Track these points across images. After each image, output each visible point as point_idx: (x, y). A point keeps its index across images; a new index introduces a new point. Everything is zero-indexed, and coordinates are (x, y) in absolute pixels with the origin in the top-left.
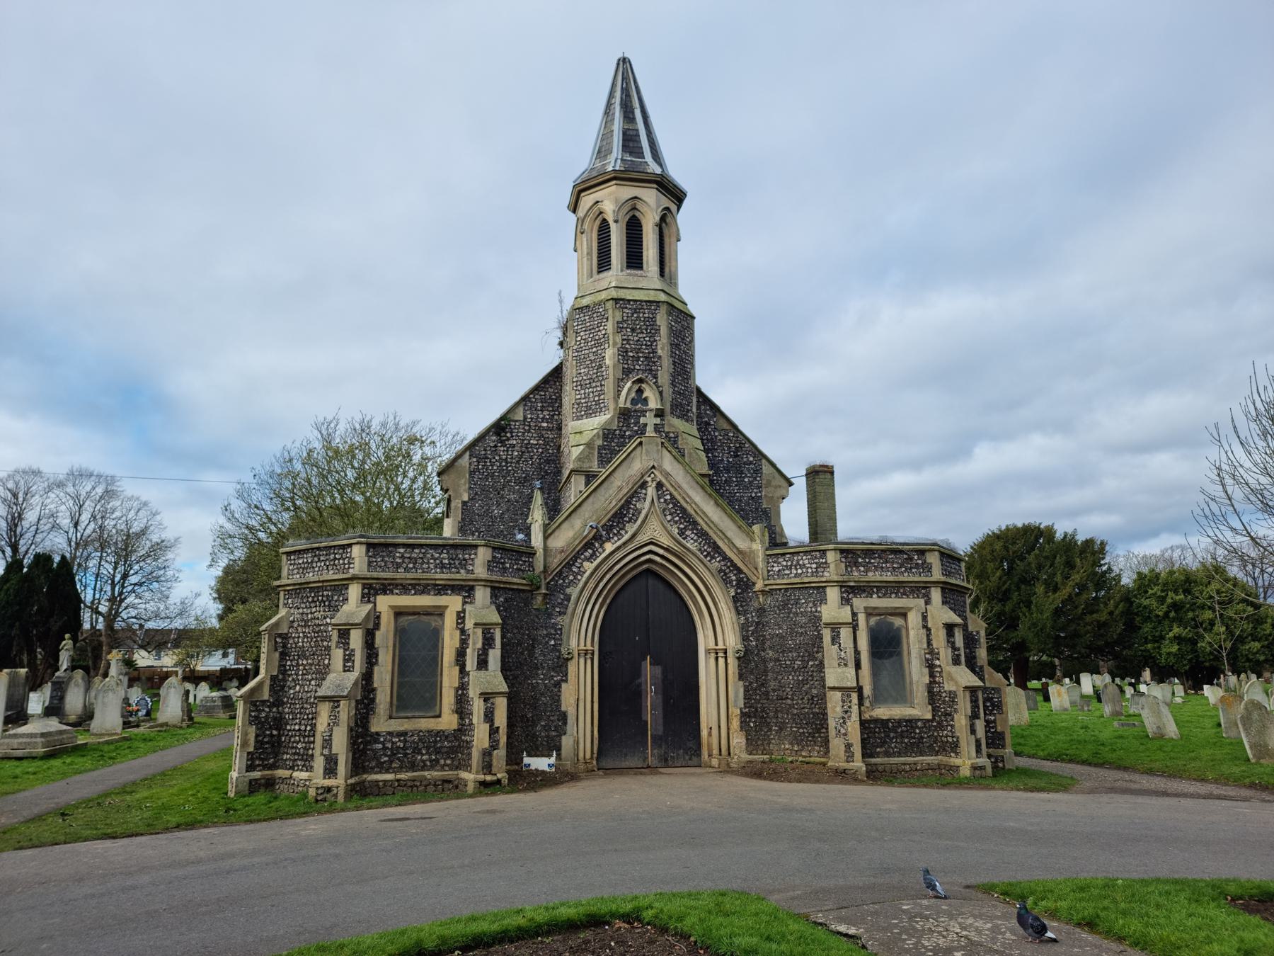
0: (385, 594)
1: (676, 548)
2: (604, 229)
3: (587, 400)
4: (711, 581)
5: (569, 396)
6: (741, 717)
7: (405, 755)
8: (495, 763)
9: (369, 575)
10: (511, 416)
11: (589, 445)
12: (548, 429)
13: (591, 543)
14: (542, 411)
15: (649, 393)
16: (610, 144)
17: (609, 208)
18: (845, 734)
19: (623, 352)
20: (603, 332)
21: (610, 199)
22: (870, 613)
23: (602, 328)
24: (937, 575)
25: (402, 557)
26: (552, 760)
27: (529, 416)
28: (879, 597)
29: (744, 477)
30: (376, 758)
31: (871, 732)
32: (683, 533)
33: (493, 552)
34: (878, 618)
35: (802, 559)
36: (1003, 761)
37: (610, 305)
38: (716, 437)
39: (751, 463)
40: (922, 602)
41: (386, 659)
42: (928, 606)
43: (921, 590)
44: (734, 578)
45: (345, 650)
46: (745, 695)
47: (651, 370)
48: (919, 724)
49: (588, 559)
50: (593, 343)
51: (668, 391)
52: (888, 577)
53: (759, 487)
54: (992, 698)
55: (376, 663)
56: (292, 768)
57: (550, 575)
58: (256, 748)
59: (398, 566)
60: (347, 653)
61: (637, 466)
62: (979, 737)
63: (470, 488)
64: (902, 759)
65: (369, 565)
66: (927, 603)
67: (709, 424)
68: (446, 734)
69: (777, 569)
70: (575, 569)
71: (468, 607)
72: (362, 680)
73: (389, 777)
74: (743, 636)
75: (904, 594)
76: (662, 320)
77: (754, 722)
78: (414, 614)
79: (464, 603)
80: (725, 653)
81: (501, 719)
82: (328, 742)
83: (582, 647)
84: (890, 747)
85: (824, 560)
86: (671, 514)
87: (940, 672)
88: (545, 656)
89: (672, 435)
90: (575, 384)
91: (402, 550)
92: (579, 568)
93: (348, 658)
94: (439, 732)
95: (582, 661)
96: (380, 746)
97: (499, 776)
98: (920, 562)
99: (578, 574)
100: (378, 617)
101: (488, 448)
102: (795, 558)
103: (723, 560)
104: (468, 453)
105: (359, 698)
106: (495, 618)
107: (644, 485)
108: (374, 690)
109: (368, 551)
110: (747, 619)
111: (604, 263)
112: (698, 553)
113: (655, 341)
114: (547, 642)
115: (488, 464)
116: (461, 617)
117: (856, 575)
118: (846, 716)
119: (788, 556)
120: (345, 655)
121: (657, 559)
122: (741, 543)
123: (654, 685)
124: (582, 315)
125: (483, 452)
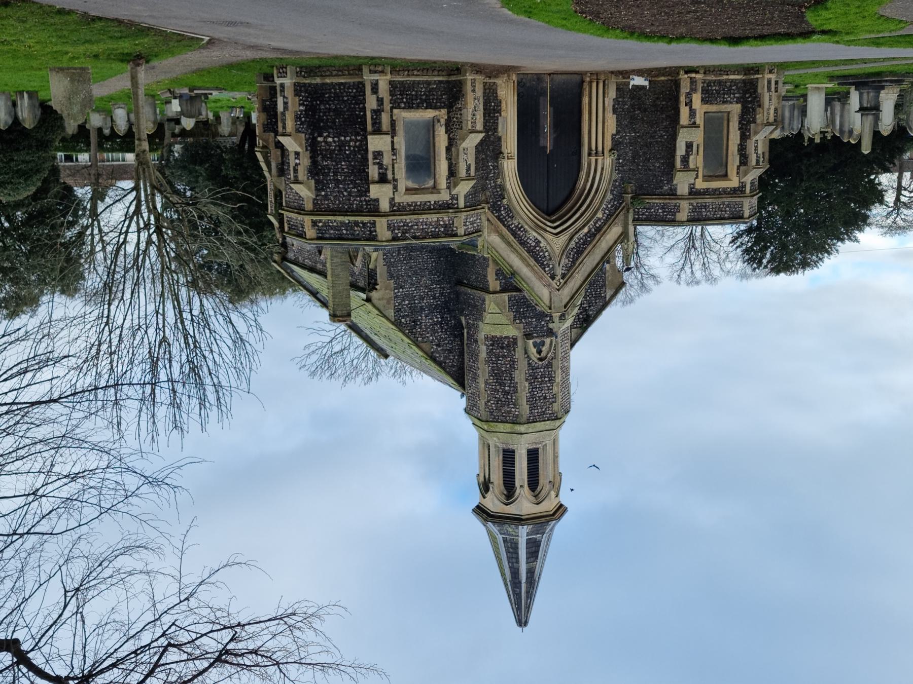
0: (734, 188)
1: (542, 232)
2: (533, 482)
6: (500, 110)
7: (723, 90)
8: (688, 84)
9: (742, 199)
10: (580, 331)
13: (598, 232)
18: (475, 99)
22: (435, 189)
24: (381, 224)
25: (726, 211)
26: (632, 83)
28: (430, 202)
29: (409, 304)
30: (738, 88)
31: (440, 99)
32: (537, 243)
33: (675, 218)
34: (426, 186)
36: (297, 73)
38: (431, 335)
39: (403, 317)
40: (397, 200)
42: (392, 196)
43: (397, 209)
44: (503, 212)
46: (497, 126)
47: (533, 369)
48: (403, 105)
49: (599, 219)
53: (396, 297)
54: (300, 124)
55: (738, 145)
57: (624, 207)
59: (728, 206)
62: (381, 96)
63: (605, 274)
64: (417, 79)
65: (742, 205)
66: (393, 199)
67: (437, 345)
70: (607, 212)
71: (693, 181)
72: (750, 135)
73: (732, 77)
74: (498, 169)
75: (410, 206)
76: (524, 409)
77: (491, 106)
79: (694, 184)
81: (684, 112)
83: (593, 159)
84: (425, 88)
86: (545, 257)
88: (625, 152)
89: (518, 321)
91: (726, 216)
95: (600, 149)
96: (736, 95)
97: (686, 76)
98: (396, 231)
99: (605, 209)
100: (738, 173)
103: (510, 225)
104: (607, 299)
105: (752, 125)
108: (739, 129)
109: (743, 214)
110: (495, 182)
111: (533, 456)
112: (529, 229)
113: (530, 393)
114: (624, 160)
117: (445, 218)
121: (549, 224)
123: (544, 133)
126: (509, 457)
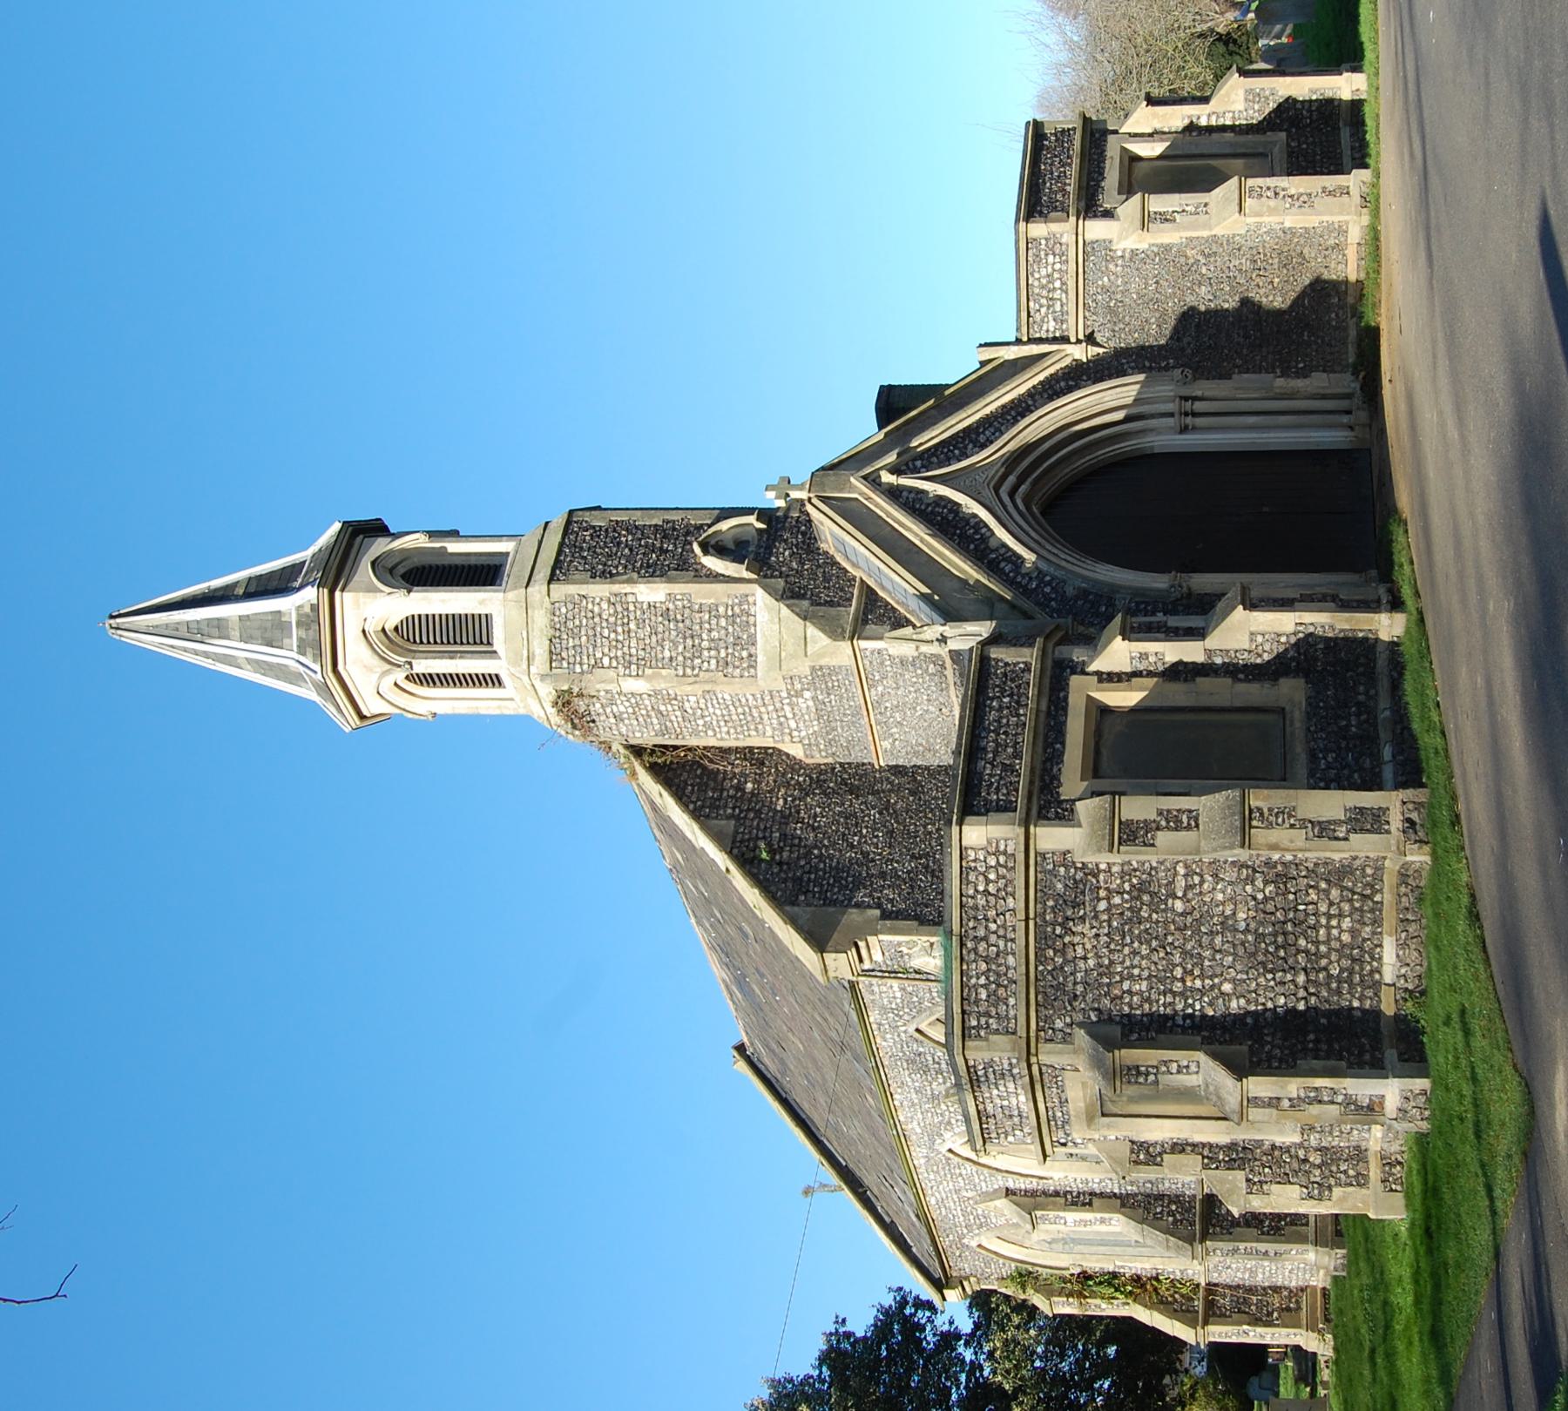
3: (722, 644)
14: (722, 790)
20: (604, 605)
23: (596, 609)
27: (729, 811)
35: (1039, 279)
45: (1158, 829)
46: (1254, 372)
50: (620, 629)
52: (1073, 171)
56: (1377, 985)
58: (1341, 1059)
60: (1163, 823)
68: (1313, 694)
69: (1052, 323)
78: (1097, 752)
80: (1186, 399)
82: (1324, 830)
85: (1043, 242)
87: (1218, 117)
90: (689, 671)
92: (1031, 579)
94: (1310, 704)
101: (783, 875)
102: (1037, 291)
115: (813, 876)
118: (1282, 193)
119: (1031, 304)
120: (1168, 828)
124: (564, 655)
125: (790, 885)
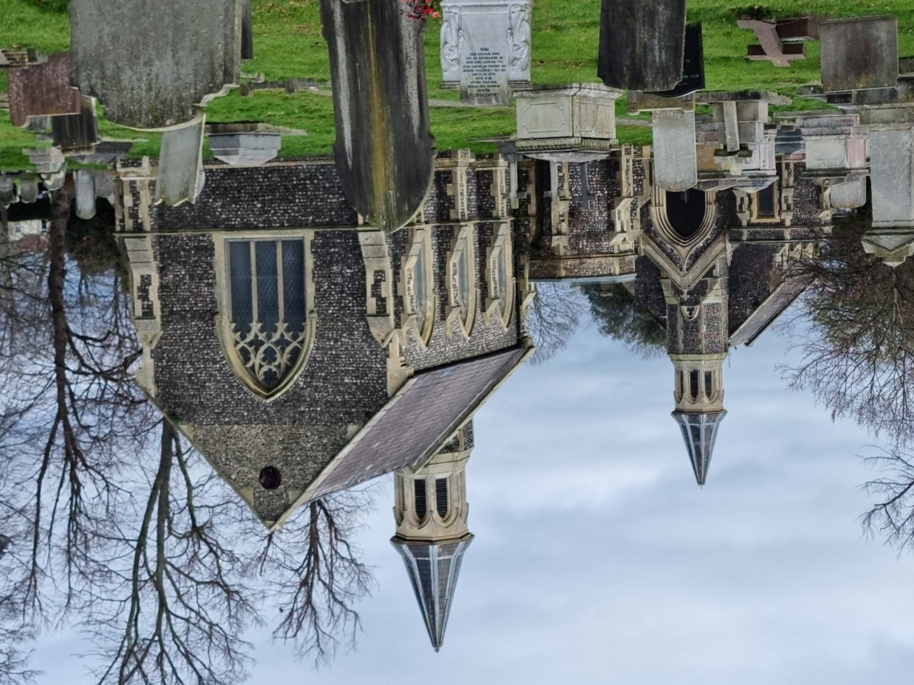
2: (442, 509)
4: (661, 232)
5: (724, 315)
11: (711, 289)
12: (735, 305)
13: (708, 245)
15: (687, 313)
16: (706, 434)
17: (705, 399)
19: (698, 330)
21: (704, 403)
37: (704, 352)
41: (776, 201)
51: (679, 315)
61: (690, 277)
76: (681, 346)
82: (789, 173)
93: (786, 200)
106: (739, 215)
107: (688, 269)
116: (751, 215)
122: (649, 248)
126: (420, 486)
